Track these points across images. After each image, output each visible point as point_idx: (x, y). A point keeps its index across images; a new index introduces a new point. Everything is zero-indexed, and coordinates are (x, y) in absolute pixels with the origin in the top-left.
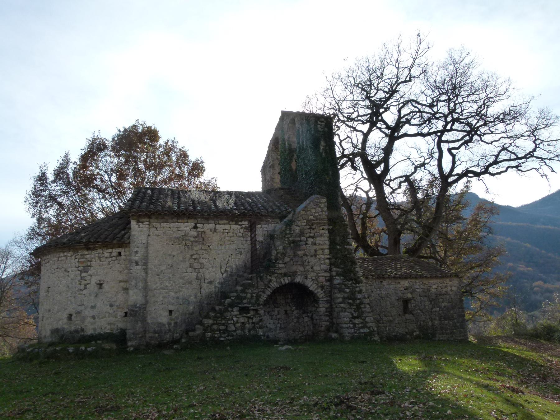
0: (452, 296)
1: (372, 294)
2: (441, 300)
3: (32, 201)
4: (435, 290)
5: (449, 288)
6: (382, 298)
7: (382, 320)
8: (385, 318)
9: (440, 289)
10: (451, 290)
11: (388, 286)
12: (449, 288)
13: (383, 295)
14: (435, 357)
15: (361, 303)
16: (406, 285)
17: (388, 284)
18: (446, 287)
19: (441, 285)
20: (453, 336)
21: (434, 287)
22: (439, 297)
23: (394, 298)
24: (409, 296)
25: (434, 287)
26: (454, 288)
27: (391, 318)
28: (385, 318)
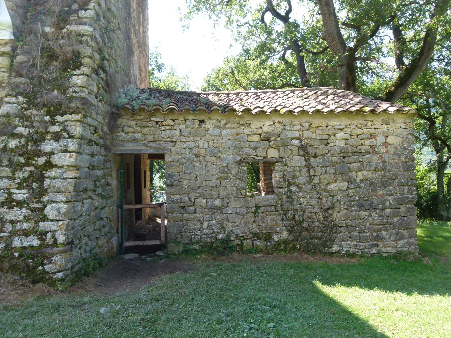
0: (386, 157)
1: (173, 149)
2: (356, 165)
3: (45, 71)
4: (343, 143)
5: (380, 140)
6: (197, 156)
7: (194, 204)
8: (201, 202)
9: (354, 141)
10: (386, 144)
11: (216, 132)
12: (380, 140)
13: (202, 152)
14: (419, 232)
15: (49, 165)
16: (266, 129)
17: (218, 127)
18: (372, 136)
19: (359, 131)
20: (377, 246)
21: (340, 135)
22: (352, 159)
23: (229, 157)
24: (273, 154)
25: (340, 135)
26: (391, 140)
27: (218, 202)
28: (201, 202)
